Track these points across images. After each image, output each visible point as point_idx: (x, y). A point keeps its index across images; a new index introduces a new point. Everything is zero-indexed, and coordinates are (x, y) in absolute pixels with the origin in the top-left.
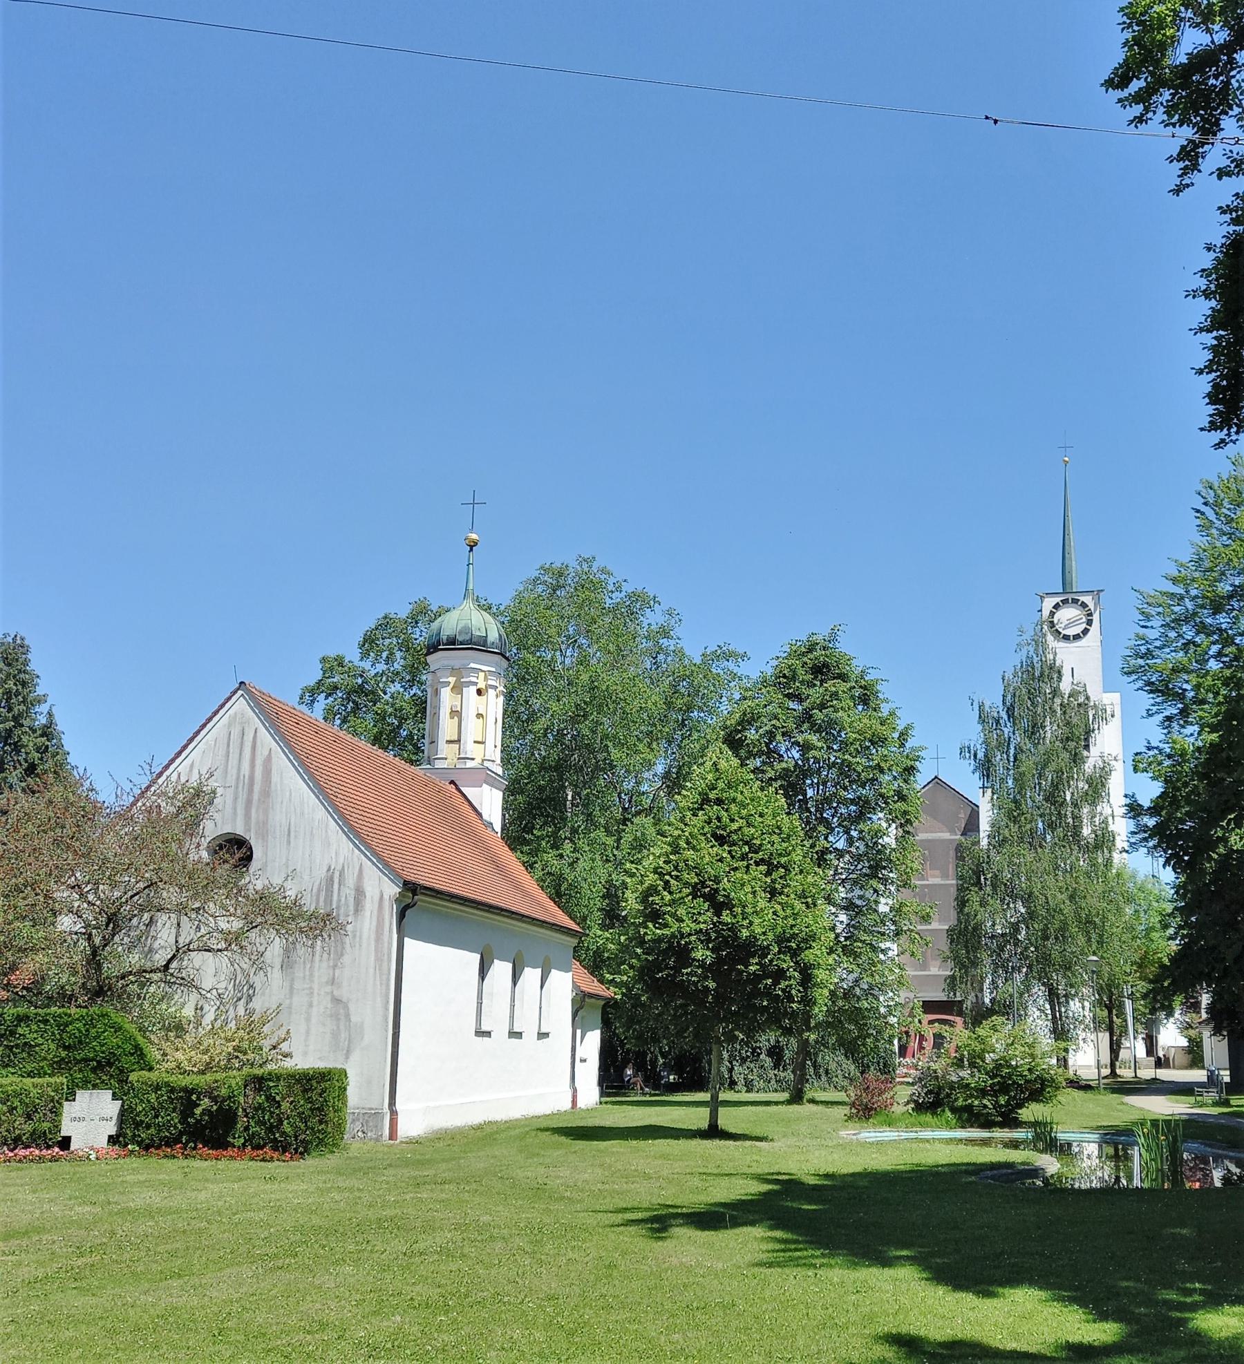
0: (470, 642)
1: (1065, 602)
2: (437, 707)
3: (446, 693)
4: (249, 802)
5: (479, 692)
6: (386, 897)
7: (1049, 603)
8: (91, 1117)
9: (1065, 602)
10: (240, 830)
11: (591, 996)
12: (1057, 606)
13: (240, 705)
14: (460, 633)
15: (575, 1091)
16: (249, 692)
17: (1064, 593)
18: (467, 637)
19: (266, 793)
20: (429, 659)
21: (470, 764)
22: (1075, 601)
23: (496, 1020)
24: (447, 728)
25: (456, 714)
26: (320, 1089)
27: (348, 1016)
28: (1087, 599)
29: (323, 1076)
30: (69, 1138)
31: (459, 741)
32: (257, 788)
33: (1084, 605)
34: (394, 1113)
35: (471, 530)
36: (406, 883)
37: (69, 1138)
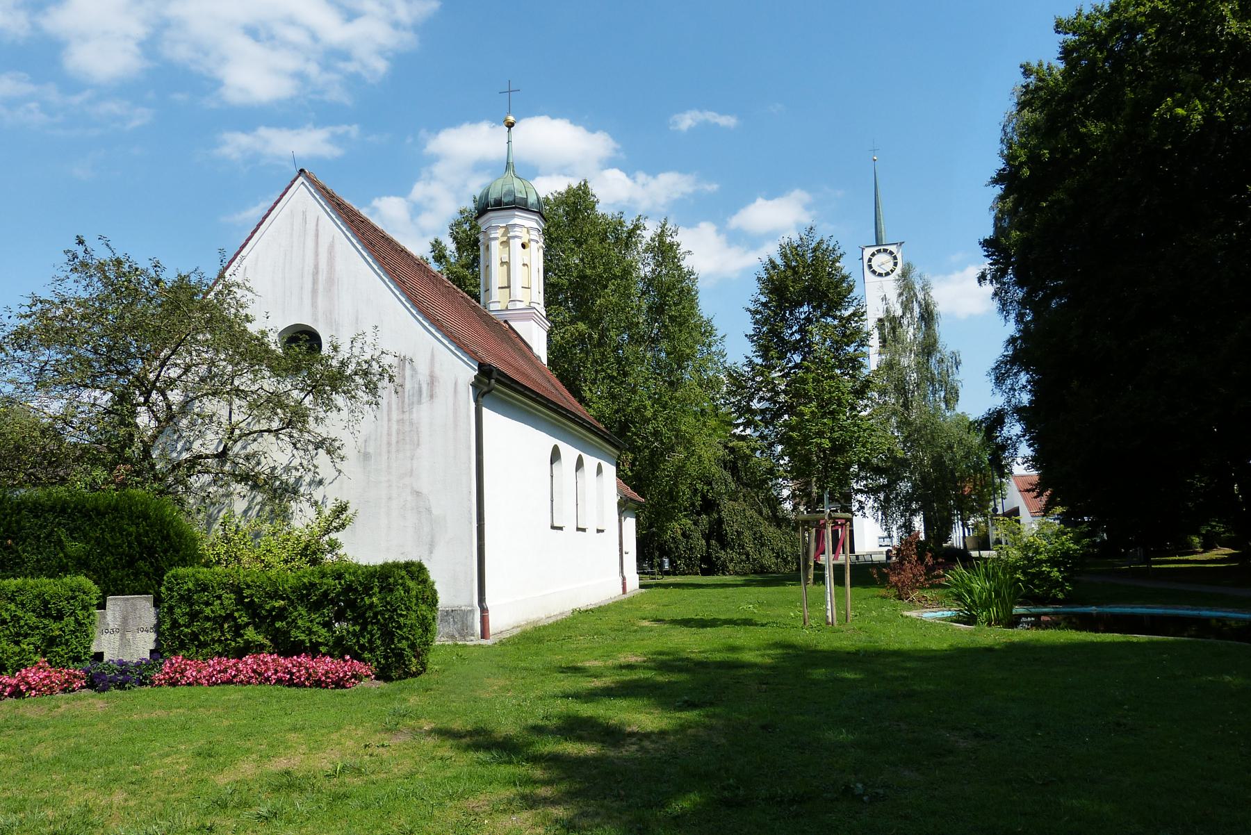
0: (514, 202)
1: (879, 251)
2: (488, 260)
3: (495, 247)
4: (314, 291)
5: (524, 246)
6: (460, 382)
7: (868, 252)
8: (125, 630)
9: (879, 251)
10: (307, 321)
11: (632, 500)
12: (873, 255)
13: (301, 194)
14: (505, 195)
15: (624, 579)
16: (308, 178)
17: (877, 245)
18: (511, 199)
19: (331, 281)
20: (480, 221)
21: (519, 305)
22: (885, 251)
23: (566, 517)
24: (497, 276)
25: (506, 263)
26: (404, 583)
27: (429, 511)
28: (893, 248)
29: (385, 576)
30: (102, 654)
31: (509, 287)
32: (322, 277)
33: (891, 253)
34: (484, 610)
35: (509, 113)
36: (482, 366)
37: (102, 654)
